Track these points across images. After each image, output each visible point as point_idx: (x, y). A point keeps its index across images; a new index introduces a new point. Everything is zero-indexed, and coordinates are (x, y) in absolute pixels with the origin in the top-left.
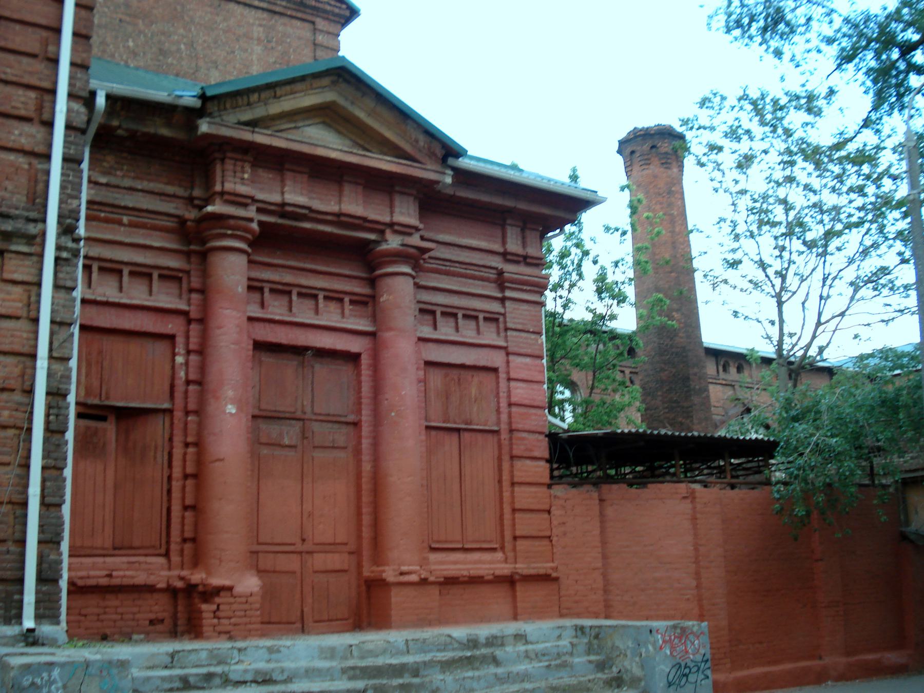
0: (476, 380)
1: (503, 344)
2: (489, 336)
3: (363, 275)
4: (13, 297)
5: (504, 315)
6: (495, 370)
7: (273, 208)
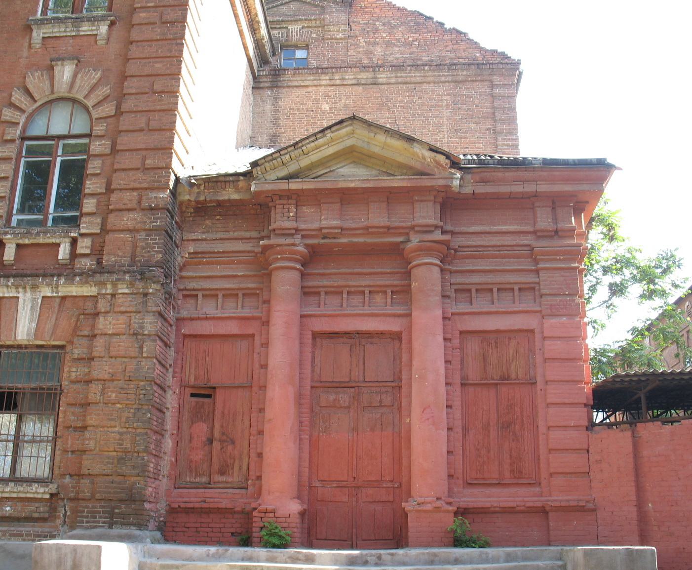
0: (513, 343)
1: (538, 309)
2: (527, 304)
3: (402, 270)
4: (120, 322)
5: (539, 283)
6: (532, 331)
7: (314, 233)
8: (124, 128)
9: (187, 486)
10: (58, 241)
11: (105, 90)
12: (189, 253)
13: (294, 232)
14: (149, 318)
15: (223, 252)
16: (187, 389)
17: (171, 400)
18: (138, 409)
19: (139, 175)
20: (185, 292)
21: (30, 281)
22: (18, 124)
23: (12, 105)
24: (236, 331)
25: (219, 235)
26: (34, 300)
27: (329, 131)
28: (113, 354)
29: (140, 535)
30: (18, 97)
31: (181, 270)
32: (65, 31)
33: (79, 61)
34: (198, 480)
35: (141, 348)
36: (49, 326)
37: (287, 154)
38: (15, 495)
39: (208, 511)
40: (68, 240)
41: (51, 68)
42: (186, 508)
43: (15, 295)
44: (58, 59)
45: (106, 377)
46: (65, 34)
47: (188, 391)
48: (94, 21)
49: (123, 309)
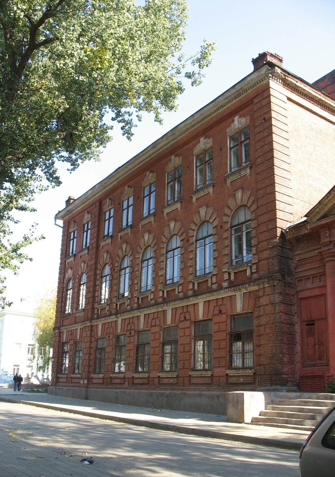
8: (260, 214)
9: (308, 366)
10: (174, 288)
11: (252, 198)
12: (297, 261)
13: (329, 243)
14: (277, 296)
15: (309, 258)
16: (304, 322)
17: (297, 328)
18: (277, 335)
19: (267, 233)
20: (298, 279)
21: (237, 288)
22: (228, 222)
23: (226, 215)
24: (318, 293)
25: (307, 250)
26: (241, 295)
27: (332, 191)
28: (266, 313)
29: (280, 389)
30: (227, 211)
31: (295, 269)
32: (237, 177)
33: (243, 188)
34: (312, 363)
35: (275, 309)
36: (246, 305)
37: (317, 208)
38: (243, 374)
39: (314, 377)
40: (248, 267)
41: (235, 195)
42: (305, 376)
43: (235, 294)
44: (236, 190)
45: (265, 323)
46: (237, 178)
47: (305, 323)
48: (245, 169)
49: (267, 293)
